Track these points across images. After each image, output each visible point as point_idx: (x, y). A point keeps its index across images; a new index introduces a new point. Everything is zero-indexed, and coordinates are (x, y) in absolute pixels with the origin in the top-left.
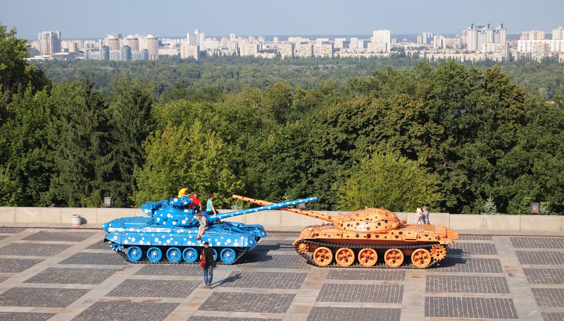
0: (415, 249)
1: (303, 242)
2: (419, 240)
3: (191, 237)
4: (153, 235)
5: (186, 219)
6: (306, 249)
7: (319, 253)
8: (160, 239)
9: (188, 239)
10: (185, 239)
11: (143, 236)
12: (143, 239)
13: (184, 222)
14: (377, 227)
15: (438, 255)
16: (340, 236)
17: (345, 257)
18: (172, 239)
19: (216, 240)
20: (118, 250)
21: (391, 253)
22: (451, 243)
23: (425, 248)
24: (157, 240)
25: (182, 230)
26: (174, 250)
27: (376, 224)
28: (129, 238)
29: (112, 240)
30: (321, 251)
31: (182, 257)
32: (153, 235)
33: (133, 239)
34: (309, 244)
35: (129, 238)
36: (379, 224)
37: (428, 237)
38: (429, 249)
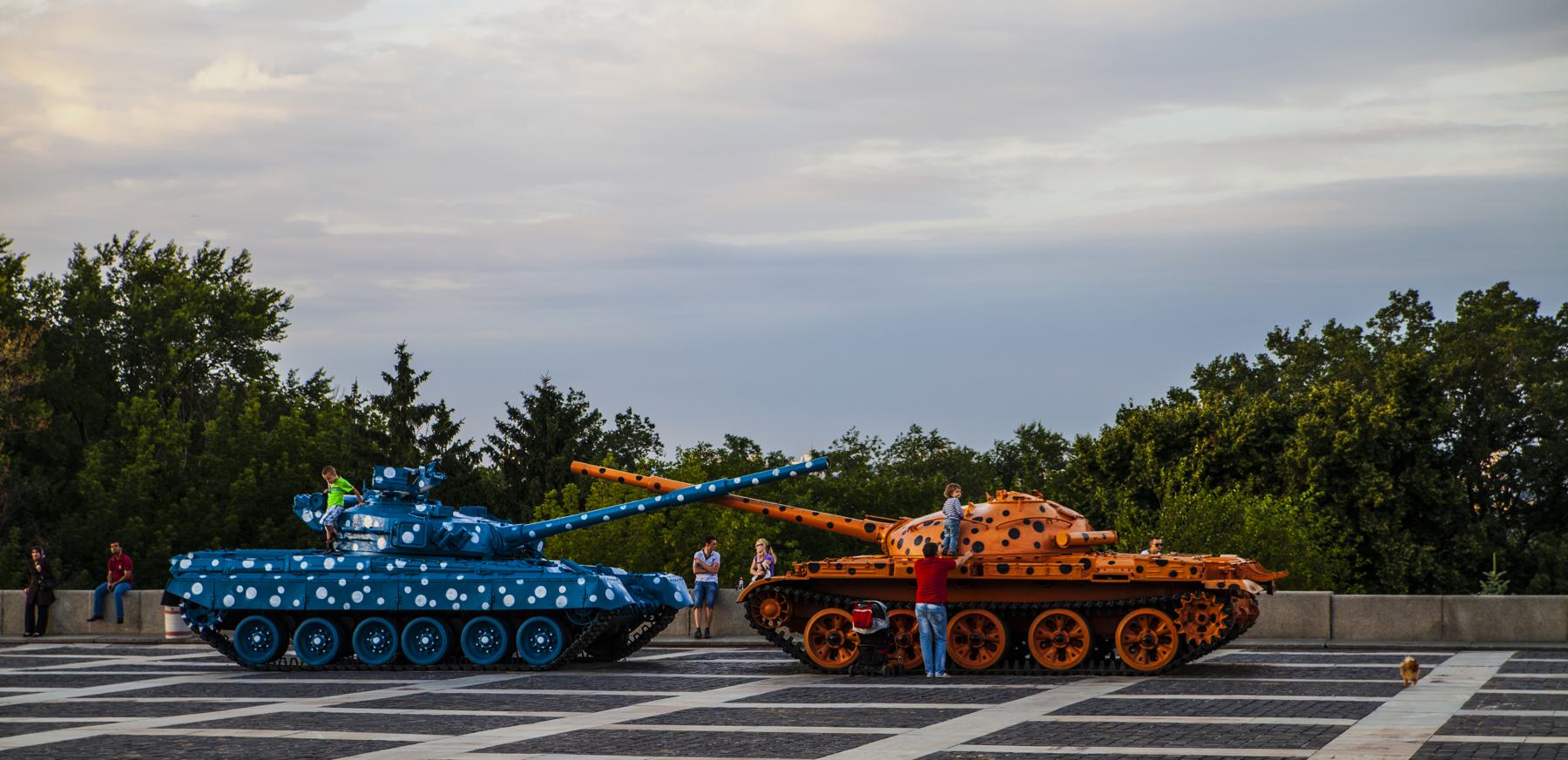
0: (1127, 609)
1: (773, 595)
2: (1141, 577)
3: (425, 582)
4: (310, 578)
5: (416, 528)
6: (783, 615)
7: (1046, 633)
8: (333, 589)
9: (418, 589)
10: (408, 590)
11: (280, 583)
12: (281, 590)
13: (408, 537)
14: (1005, 543)
15: (1202, 629)
16: (887, 570)
17: (976, 641)
18: (367, 589)
19: (502, 590)
20: (206, 629)
21: (1050, 623)
22: (565, 397)
23: (1157, 606)
24: (321, 593)
25: (401, 564)
26: (378, 626)
27: (1005, 535)
28: (240, 589)
29: (187, 596)
30: (827, 621)
31: (399, 649)
32: (310, 578)
33: (251, 593)
34: (791, 597)
35: (240, 589)
36: (1014, 534)
37: (1169, 568)
38: (1170, 608)
